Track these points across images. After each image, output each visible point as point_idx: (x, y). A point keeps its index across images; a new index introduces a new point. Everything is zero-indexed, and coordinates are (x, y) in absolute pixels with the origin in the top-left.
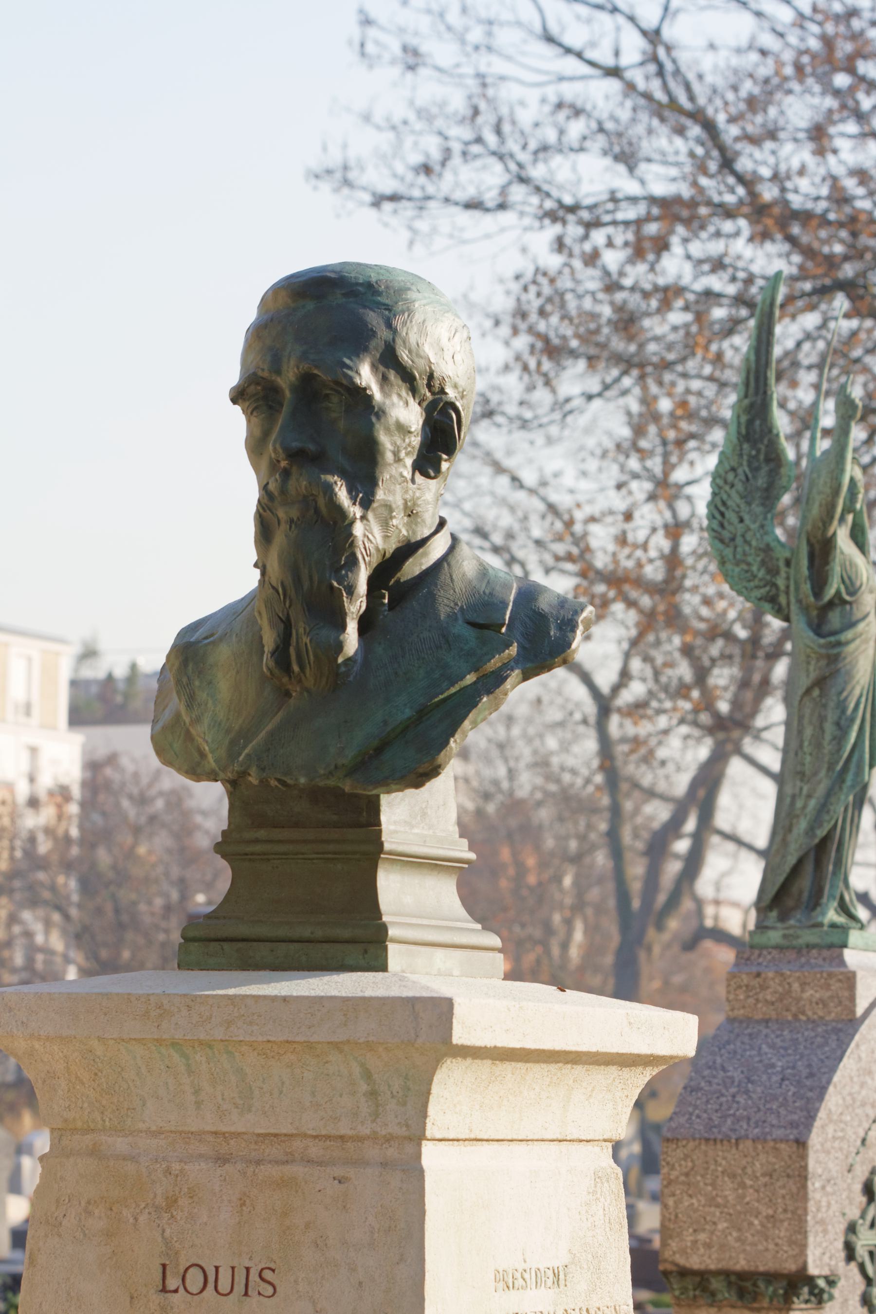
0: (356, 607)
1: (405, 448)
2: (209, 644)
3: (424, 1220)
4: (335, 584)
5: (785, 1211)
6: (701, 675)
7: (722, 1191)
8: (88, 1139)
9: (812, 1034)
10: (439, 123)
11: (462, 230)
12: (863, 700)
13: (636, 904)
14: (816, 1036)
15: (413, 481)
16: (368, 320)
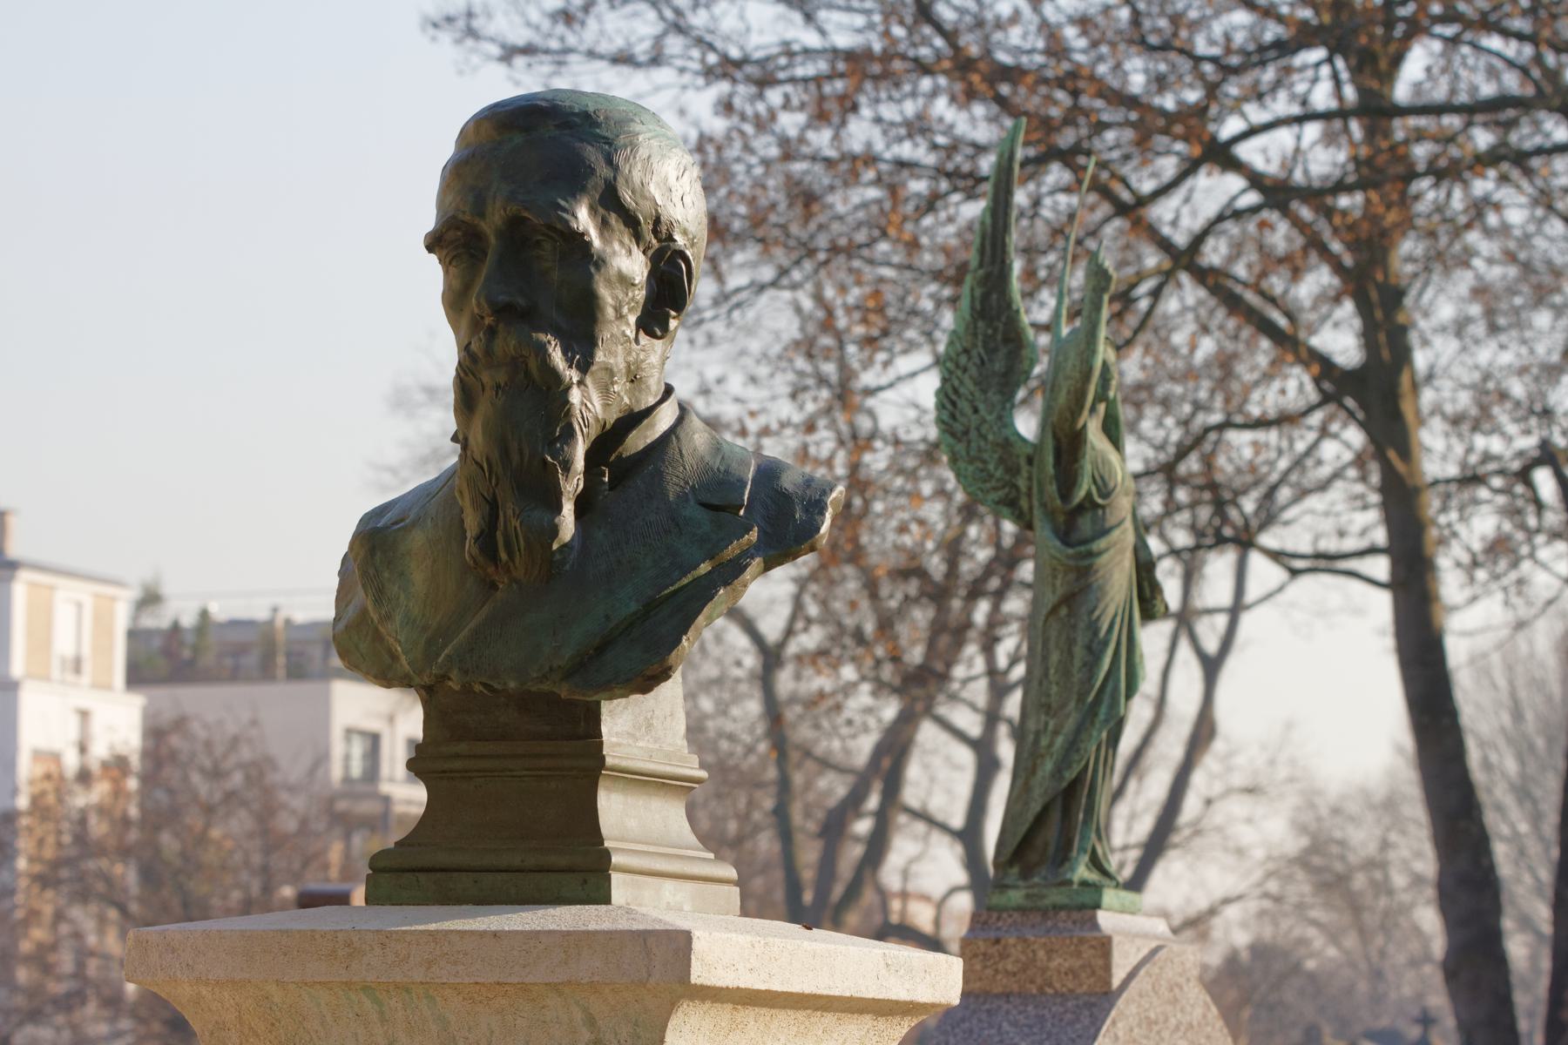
0: (572, 485)
6: (886, 625)
12: (1118, 620)
15: (637, 340)
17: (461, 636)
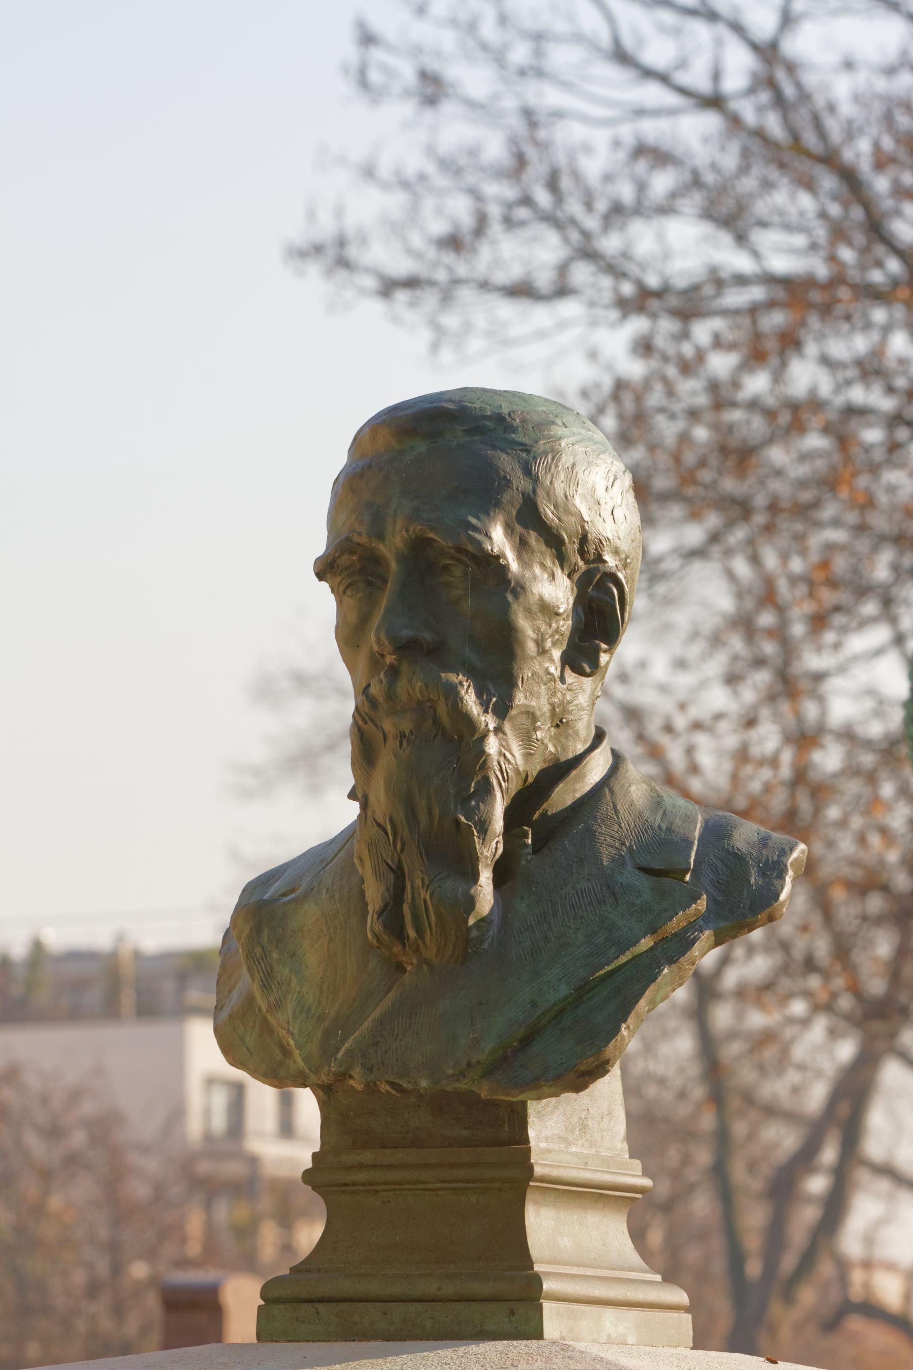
0: (490, 849)
1: (552, 636)
4: (463, 819)
6: (842, 952)
13: (754, 1269)
15: (562, 679)
16: (500, 464)
17: (365, 1026)
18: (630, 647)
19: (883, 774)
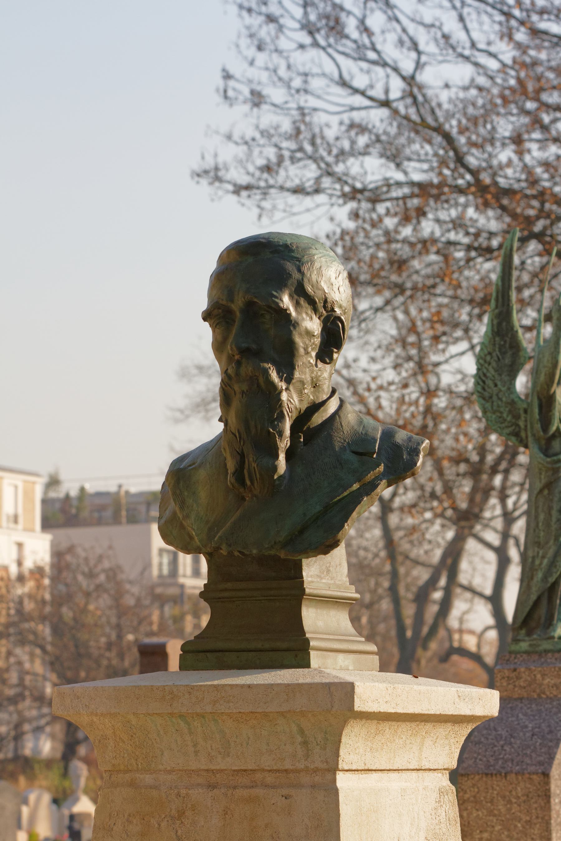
0: (284, 444)
1: (311, 346)
2: (192, 469)
3: (339, 819)
4: (271, 430)
5: (537, 817)
6: (448, 489)
7: (497, 806)
8: (128, 776)
9: (550, 706)
10: (275, 139)
11: (291, 206)
13: (409, 634)
14: (553, 708)
18: (348, 351)
19: (465, 408)
